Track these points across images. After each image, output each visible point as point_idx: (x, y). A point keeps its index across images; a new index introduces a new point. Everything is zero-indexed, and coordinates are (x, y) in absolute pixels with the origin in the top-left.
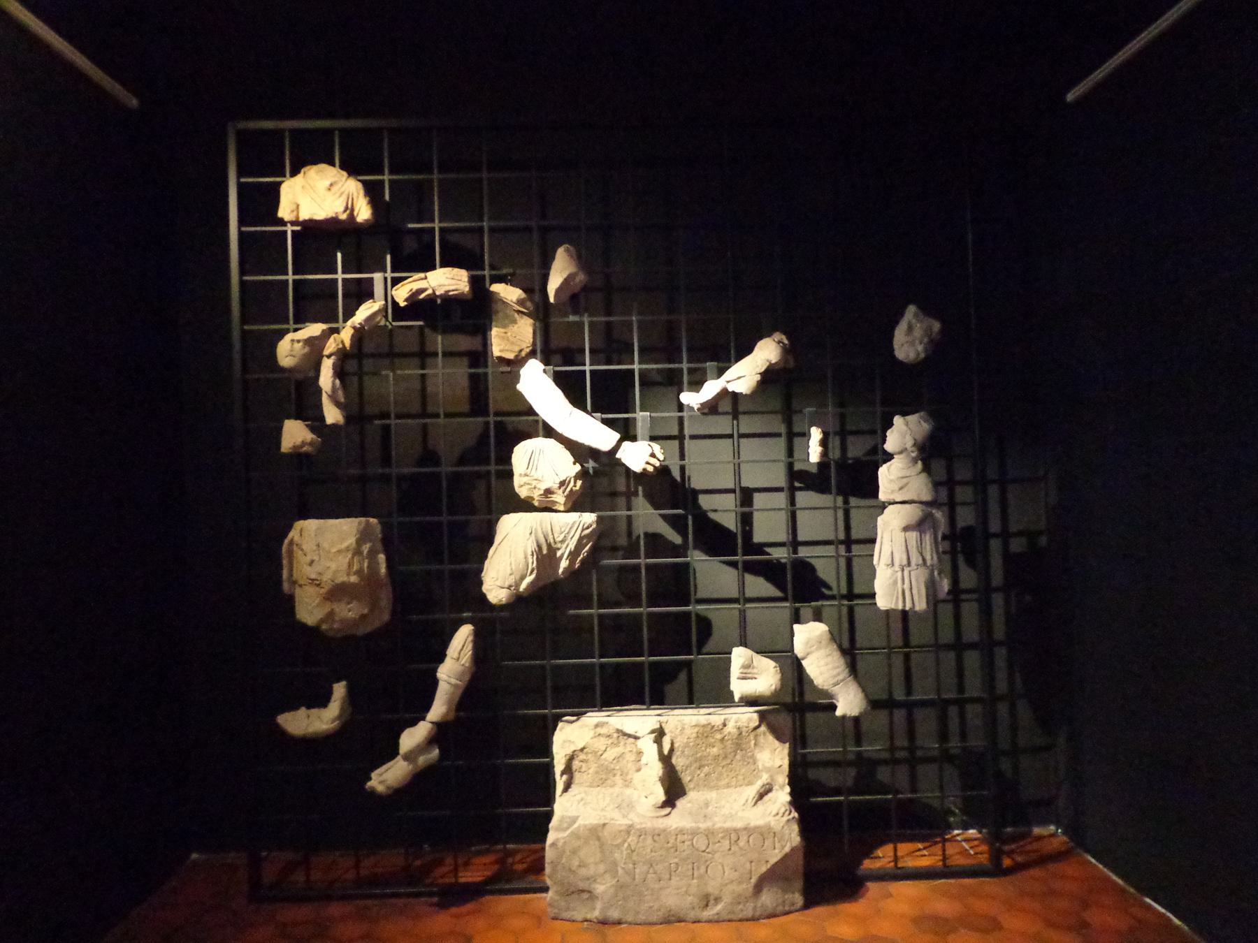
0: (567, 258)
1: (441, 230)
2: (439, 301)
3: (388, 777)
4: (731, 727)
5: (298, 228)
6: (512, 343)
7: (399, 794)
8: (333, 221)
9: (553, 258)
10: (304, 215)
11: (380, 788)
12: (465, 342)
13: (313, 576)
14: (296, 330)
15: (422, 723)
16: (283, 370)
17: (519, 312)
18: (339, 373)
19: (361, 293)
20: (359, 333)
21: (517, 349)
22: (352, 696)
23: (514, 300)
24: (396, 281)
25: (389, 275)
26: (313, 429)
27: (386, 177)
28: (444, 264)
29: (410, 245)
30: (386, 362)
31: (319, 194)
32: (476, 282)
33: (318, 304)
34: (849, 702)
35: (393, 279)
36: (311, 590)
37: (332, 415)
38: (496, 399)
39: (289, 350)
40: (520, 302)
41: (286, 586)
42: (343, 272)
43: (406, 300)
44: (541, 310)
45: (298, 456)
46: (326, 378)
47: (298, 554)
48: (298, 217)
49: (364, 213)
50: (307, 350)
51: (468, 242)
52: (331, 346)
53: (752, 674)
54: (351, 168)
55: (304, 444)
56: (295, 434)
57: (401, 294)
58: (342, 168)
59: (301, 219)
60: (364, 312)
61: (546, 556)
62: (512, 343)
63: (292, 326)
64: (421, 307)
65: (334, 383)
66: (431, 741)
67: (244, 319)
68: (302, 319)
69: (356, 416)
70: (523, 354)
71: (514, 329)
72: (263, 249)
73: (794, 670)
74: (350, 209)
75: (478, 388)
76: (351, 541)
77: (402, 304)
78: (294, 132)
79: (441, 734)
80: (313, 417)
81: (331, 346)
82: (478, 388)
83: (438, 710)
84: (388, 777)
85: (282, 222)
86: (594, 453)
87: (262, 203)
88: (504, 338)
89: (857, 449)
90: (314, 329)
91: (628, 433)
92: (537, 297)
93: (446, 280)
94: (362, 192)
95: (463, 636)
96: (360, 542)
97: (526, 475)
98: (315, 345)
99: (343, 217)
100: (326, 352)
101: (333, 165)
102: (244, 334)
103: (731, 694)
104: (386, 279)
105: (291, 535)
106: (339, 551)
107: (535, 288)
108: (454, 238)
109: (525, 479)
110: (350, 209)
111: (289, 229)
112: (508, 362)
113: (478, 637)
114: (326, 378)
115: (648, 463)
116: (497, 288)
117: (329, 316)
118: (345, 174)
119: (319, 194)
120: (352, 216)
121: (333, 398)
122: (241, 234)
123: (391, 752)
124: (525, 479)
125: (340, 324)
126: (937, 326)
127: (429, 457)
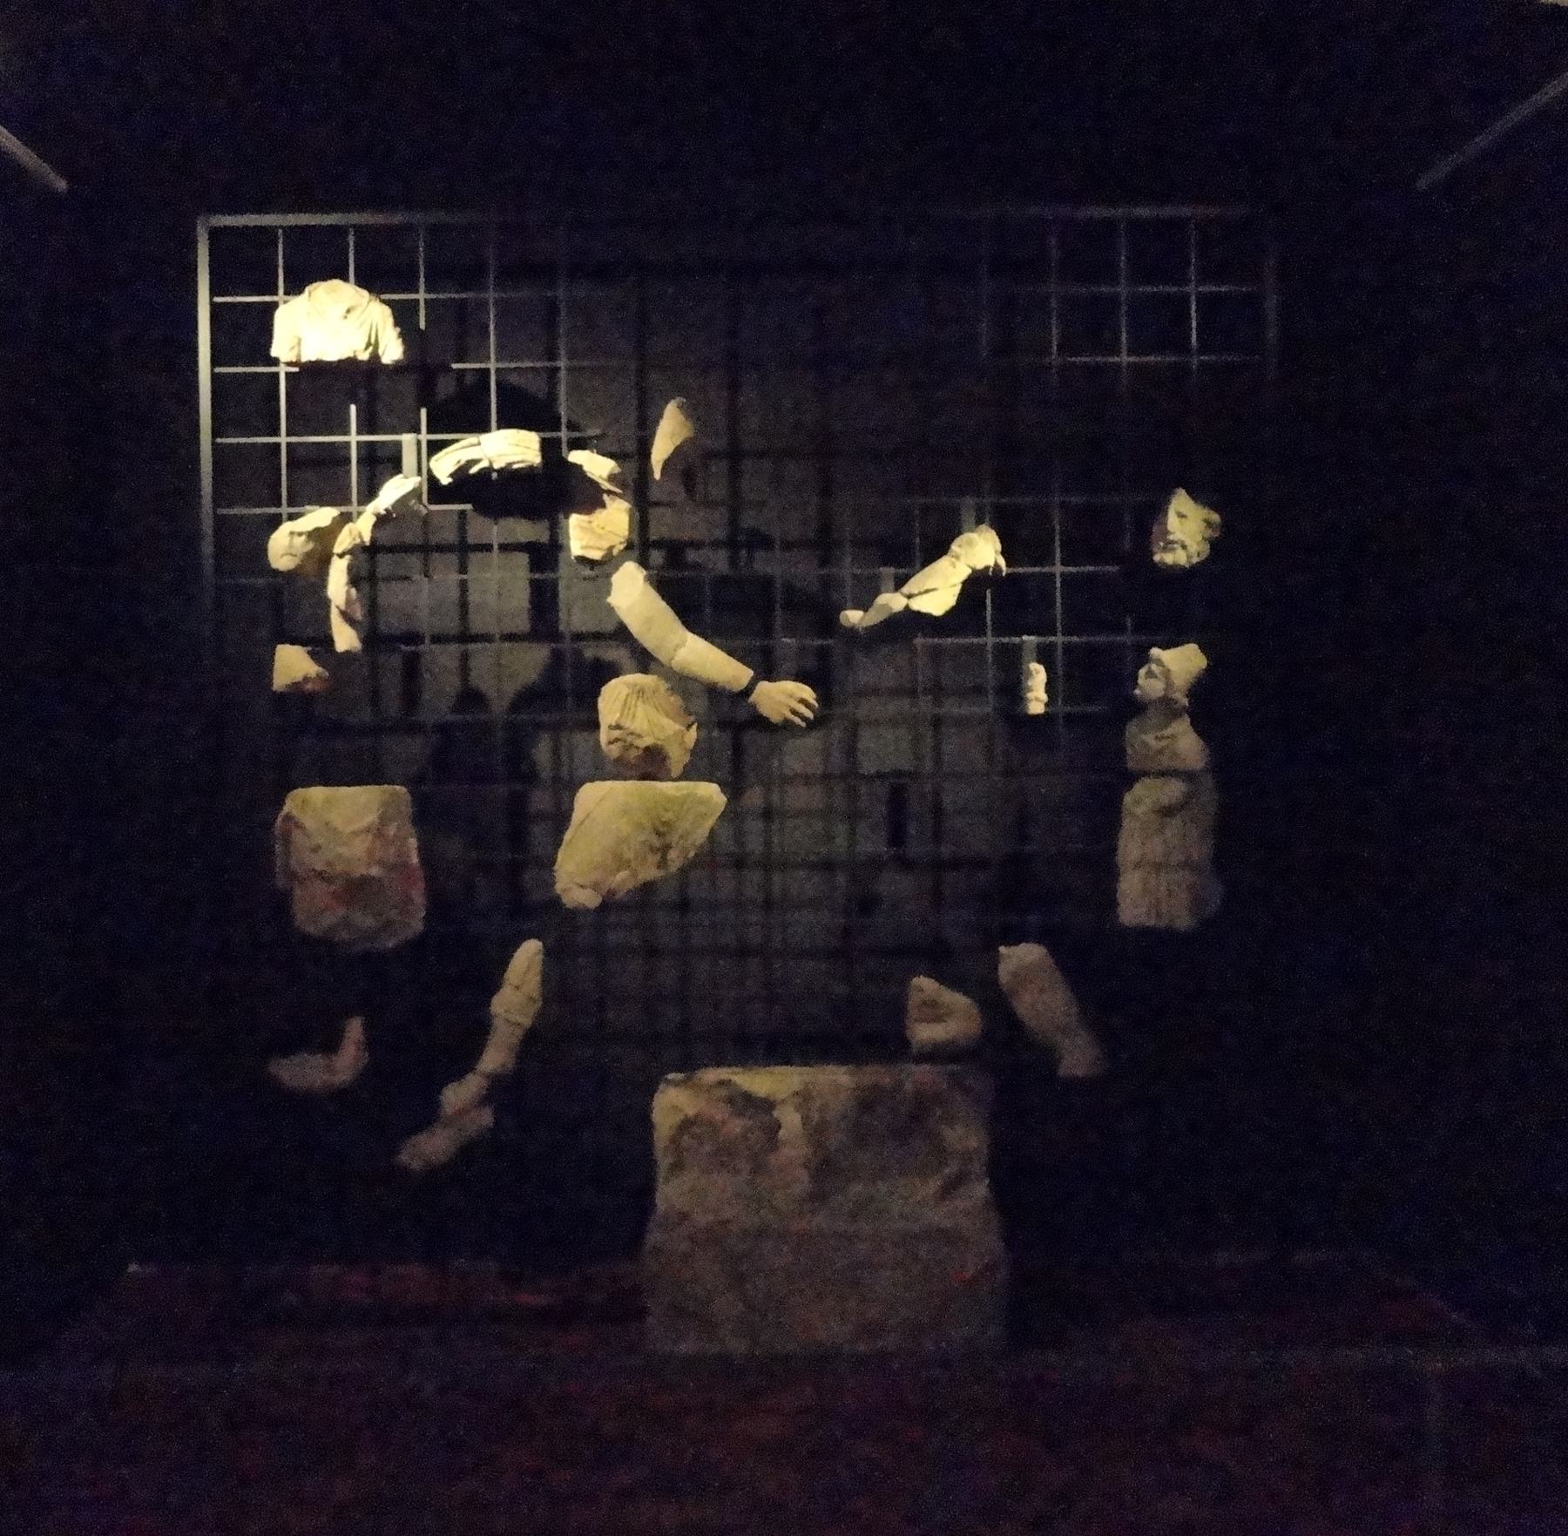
0: (681, 418)
1: (498, 370)
2: (495, 475)
3: (430, 1147)
4: (908, 1087)
5: (296, 369)
6: (600, 537)
7: (436, 1177)
8: (350, 363)
9: (661, 416)
10: (308, 356)
11: (416, 1165)
12: (525, 530)
13: (319, 867)
14: (292, 517)
15: (470, 1076)
16: (276, 573)
17: (609, 492)
18: (354, 580)
19: (380, 464)
20: (382, 521)
21: (606, 545)
22: (371, 1043)
23: (605, 474)
24: (435, 447)
25: (424, 437)
26: (313, 655)
27: (421, 296)
28: (505, 423)
29: (445, 388)
30: (414, 560)
31: (331, 322)
32: (549, 447)
33: (322, 477)
34: (1078, 1057)
35: (429, 442)
36: (319, 888)
37: (345, 638)
38: (574, 617)
39: (285, 545)
40: (612, 478)
41: (281, 882)
42: (359, 432)
43: (451, 475)
44: (637, 486)
45: (298, 694)
46: (338, 584)
47: (297, 836)
48: (299, 356)
49: (392, 351)
50: (311, 546)
51: (537, 387)
52: (344, 541)
53: (941, 1014)
54: (370, 281)
55: (306, 679)
56: (292, 664)
57: (444, 467)
58: (362, 282)
59: (304, 359)
60: (393, 491)
61: (661, 834)
62: (600, 537)
63: (285, 510)
64: (475, 487)
65: (348, 592)
66: (485, 1100)
67: (217, 502)
68: (301, 498)
69: (373, 638)
70: (615, 552)
71: (600, 516)
72: (247, 401)
73: (995, 1004)
74: (373, 345)
75: (544, 599)
76: (371, 818)
77: (445, 480)
78: (290, 231)
79: (500, 1091)
80: (320, 644)
81: (344, 541)
82: (544, 599)
83: (495, 1058)
84: (430, 1147)
85: (275, 362)
86: (713, 691)
87: (247, 333)
88: (588, 530)
89: (609, 768)
90: (321, 516)
91: (767, 669)
92: (632, 465)
93: (509, 448)
94: (390, 320)
95: (529, 954)
96: (384, 820)
97: (618, 727)
98: (322, 538)
99: (364, 356)
100: (338, 549)
101: (345, 279)
102: (220, 522)
103: (593, 484)
104: (419, 443)
105: (286, 809)
106: (355, 834)
107: (634, 454)
108: (514, 379)
109: (617, 733)
110: (373, 345)
111: (282, 370)
112: (591, 563)
113: (552, 954)
114: (338, 584)
115: (794, 712)
116: (576, 457)
117: (333, 494)
118: (365, 293)
119: (331, 322)
120: (375, 357)
121: (347, 617)
122: (215, 378)
123: (427, 1115)
124: (617, 733)
125: (354, 508)
126: (1215, 517)
127: (471, 698)
